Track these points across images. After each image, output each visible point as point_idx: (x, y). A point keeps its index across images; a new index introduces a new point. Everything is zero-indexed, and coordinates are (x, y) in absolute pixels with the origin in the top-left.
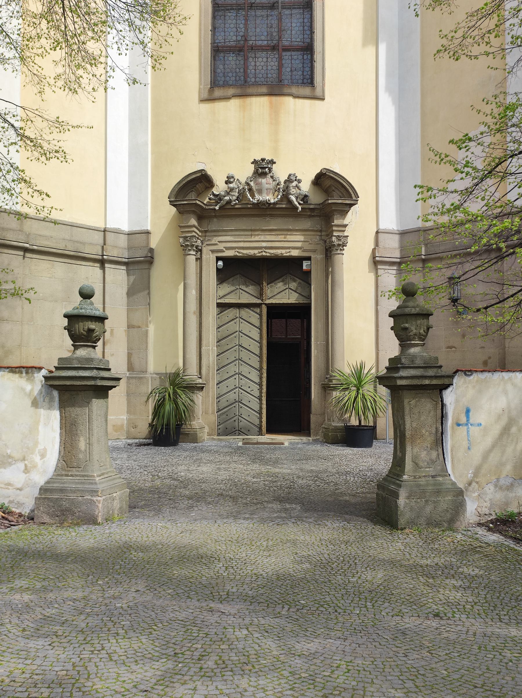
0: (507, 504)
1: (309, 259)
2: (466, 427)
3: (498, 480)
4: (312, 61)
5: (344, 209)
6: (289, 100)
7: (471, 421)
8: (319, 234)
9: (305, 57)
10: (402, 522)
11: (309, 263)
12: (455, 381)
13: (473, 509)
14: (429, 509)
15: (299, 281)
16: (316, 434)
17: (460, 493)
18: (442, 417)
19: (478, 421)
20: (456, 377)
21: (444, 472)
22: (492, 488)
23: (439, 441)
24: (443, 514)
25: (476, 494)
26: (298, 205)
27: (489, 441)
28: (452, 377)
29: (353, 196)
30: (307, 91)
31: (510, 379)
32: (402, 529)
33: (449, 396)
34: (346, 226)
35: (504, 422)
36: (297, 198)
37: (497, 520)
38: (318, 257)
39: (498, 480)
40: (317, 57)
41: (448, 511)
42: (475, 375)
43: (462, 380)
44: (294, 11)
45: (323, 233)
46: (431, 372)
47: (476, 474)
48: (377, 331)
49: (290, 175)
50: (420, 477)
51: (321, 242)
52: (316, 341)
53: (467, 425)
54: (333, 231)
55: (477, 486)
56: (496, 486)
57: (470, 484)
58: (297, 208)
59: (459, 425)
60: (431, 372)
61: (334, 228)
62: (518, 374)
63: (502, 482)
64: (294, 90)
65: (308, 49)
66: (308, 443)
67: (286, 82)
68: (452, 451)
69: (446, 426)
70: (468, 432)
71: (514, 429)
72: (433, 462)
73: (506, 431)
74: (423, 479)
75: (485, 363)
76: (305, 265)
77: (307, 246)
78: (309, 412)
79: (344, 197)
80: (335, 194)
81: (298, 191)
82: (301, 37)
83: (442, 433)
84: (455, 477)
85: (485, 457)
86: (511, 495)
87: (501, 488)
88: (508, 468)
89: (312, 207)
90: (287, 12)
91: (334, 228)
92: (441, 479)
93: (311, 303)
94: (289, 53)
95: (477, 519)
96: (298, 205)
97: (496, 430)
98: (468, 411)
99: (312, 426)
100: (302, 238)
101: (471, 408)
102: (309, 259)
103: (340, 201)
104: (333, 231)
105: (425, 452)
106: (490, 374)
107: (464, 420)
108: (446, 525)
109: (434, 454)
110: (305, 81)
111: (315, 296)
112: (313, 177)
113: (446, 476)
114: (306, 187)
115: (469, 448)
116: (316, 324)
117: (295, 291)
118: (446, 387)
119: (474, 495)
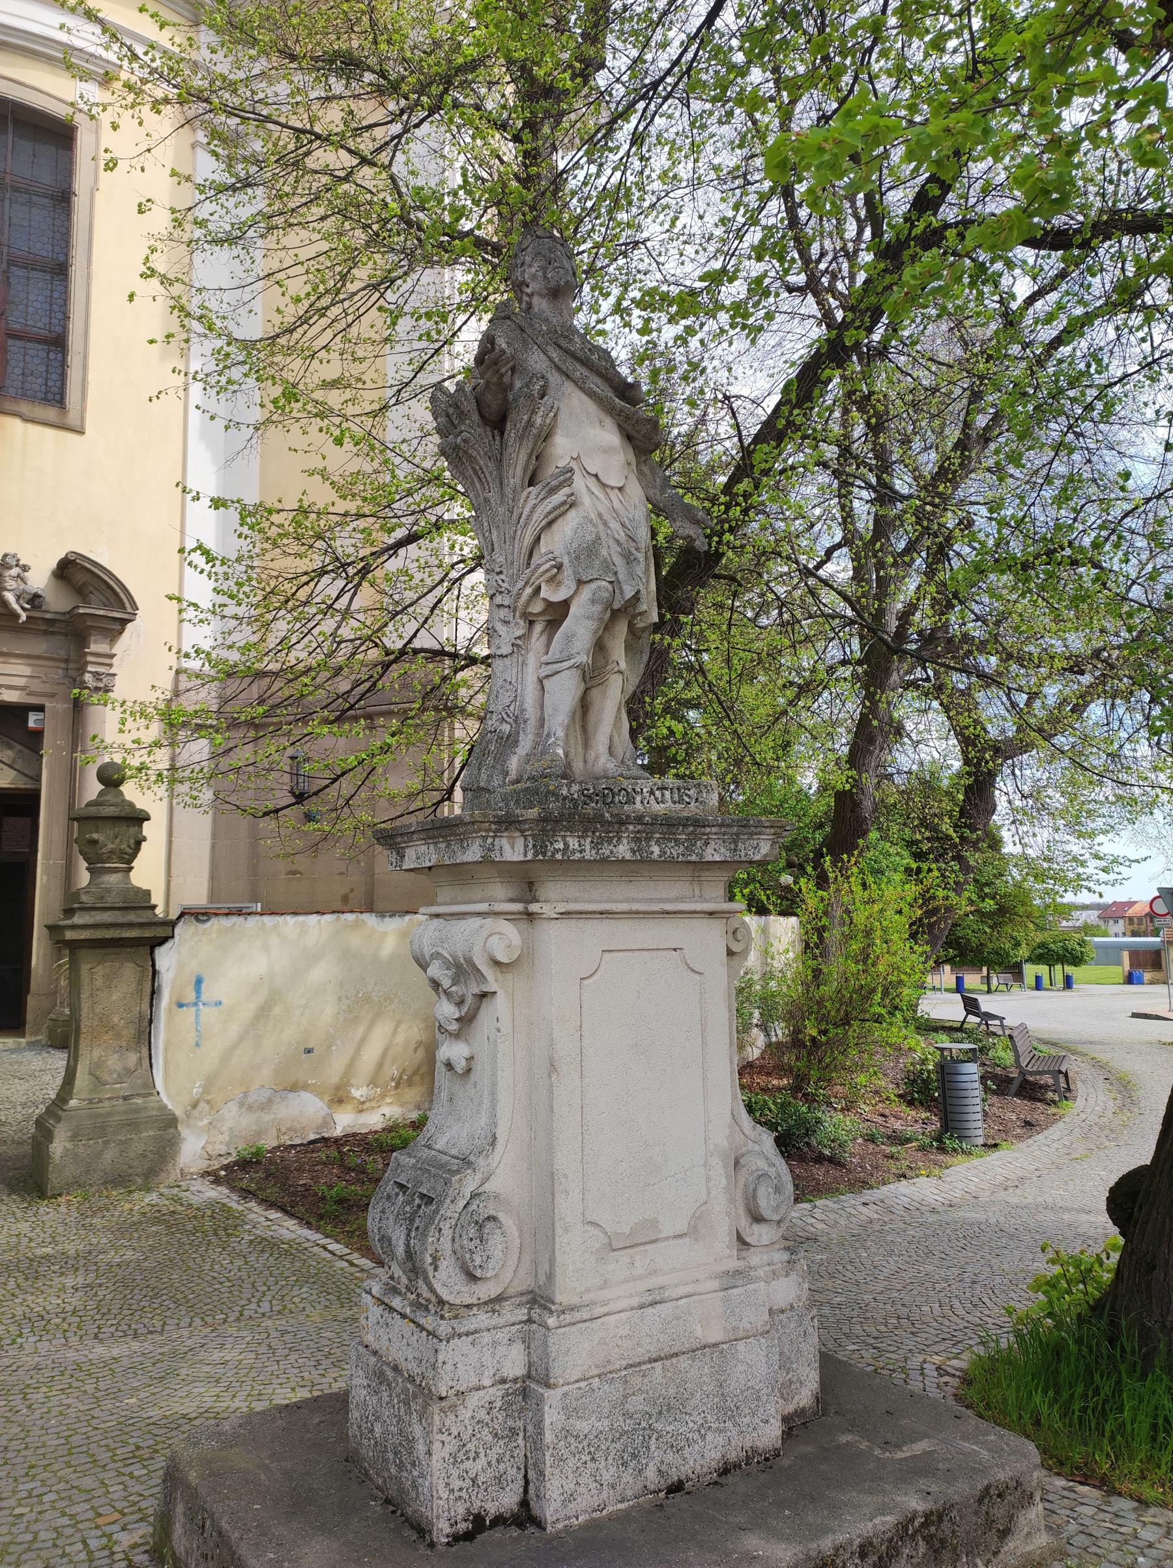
0: (259, 1134)
1: (40, 708)
2: (193, 1009)
3: (246, 1094)
4: (64, 364)
5: (116, 627)
6: (17, 423)
7: (204, 998)
8: (63, 665)
9: (52, 355)
10: (54, 1180)
11: (40, 716)
12: (177, 931)
13: (195, 1149)
14: (109, 1155)
15: (19, 747)
16: (36, 1033)
17: (170, 1122)
18: (153, 992)
19: (216, 999)
20: (180, 924)
21: (149, 1087)
22: (233, 1107)
23: (144, 1033)
24: (135, 1163)
25: (205, 1122)
26: (19, 610)
27: (234, 1030)
28: (173, 924)
29: (127, 605)
30: (51, 413)
31: (275, 926)
32: (54, 1196)
33: (165, 958)
34: (112, 656)
35: (262, 996)
36: (18, 598)
37: (236, 1163)
38: (57, 707)
39: (246, 1094)
40: (74, 360)
41: (145, 1156)
42: (214, 920)
43: (192, 929)
44: (33, 274)
45: (71, 666)
46: (132, 917)
47: (206, 1089)
48: (170, 842)
49: (5, 556)
50: (100, 1101)
51: (66, 681)
52: (47, 857)
53: (196, 1004)
54: (87, 663)
55: (207, 1108)
56: (241, 1105)
57: (195, 1106)
58: (18, 616)
59: (181, 1005)
60: (132, 917)
61: (89, 658)
62: (288, 918)
63: (253, 1097)
64: (25, 408)
65: (58, 343)
66: (17, 1050)
67: (12, 391)
68: (166, 1050)
69: (158, 1008)
70: (197, 1016)
71: (278, 1010)
72: (129, 1072)
73: (263, 1012)
74: (107, 1104)
75: (345, 899)
76: (33, 721)
77: (37, 686)
78: (28, 991)
79: (111, 605)
80: (93, 598)
81: (22, 586)
82: (46, 320)
83: (151, 1021)
84: (169, 1096)
85: (226, 1057)
86: (267, 1117)
87: (250, 1108)
88: (266, 1073)
89: (48, 616)
90: (20, 272)
91: (89, 658)
92: (139, 1101)
93: (39, 790)
94: (19, 343)
95: (203, 1165)
96: (19, 610)
97: (248, 1010)
98: (199, 982)
99: (29, 1016)
100: (27, 671)
101: (204, 975)
102: (40, 708)
103: (101, 612)
104: (87, 663)
105: (116, 1056)
106: (241, 919)
107: (191, 996)
108: (139, 1181)
109: (132, 1059)
110: (50, 396)
111: (49, 775)
112: (53, 564)
113: (151, 1094)
114: (39, 578)
115: (197, 1045)
116: (49, 826)
117: (11, 767)
118: (163, 941)
119: (201, 1124)
